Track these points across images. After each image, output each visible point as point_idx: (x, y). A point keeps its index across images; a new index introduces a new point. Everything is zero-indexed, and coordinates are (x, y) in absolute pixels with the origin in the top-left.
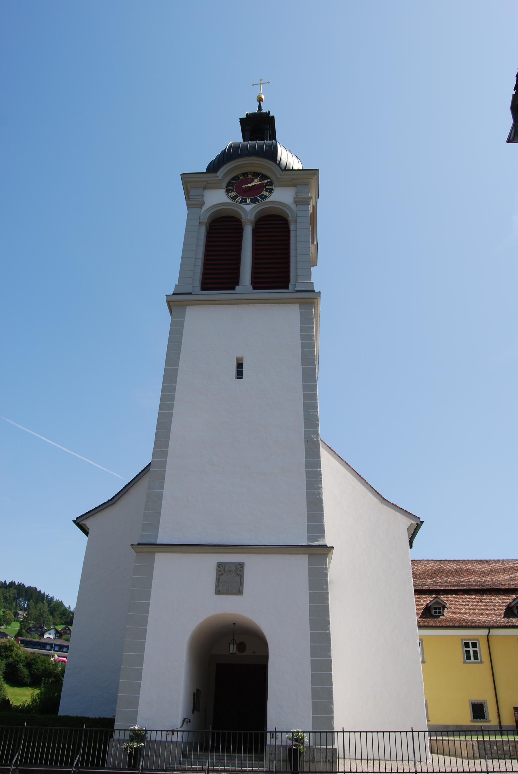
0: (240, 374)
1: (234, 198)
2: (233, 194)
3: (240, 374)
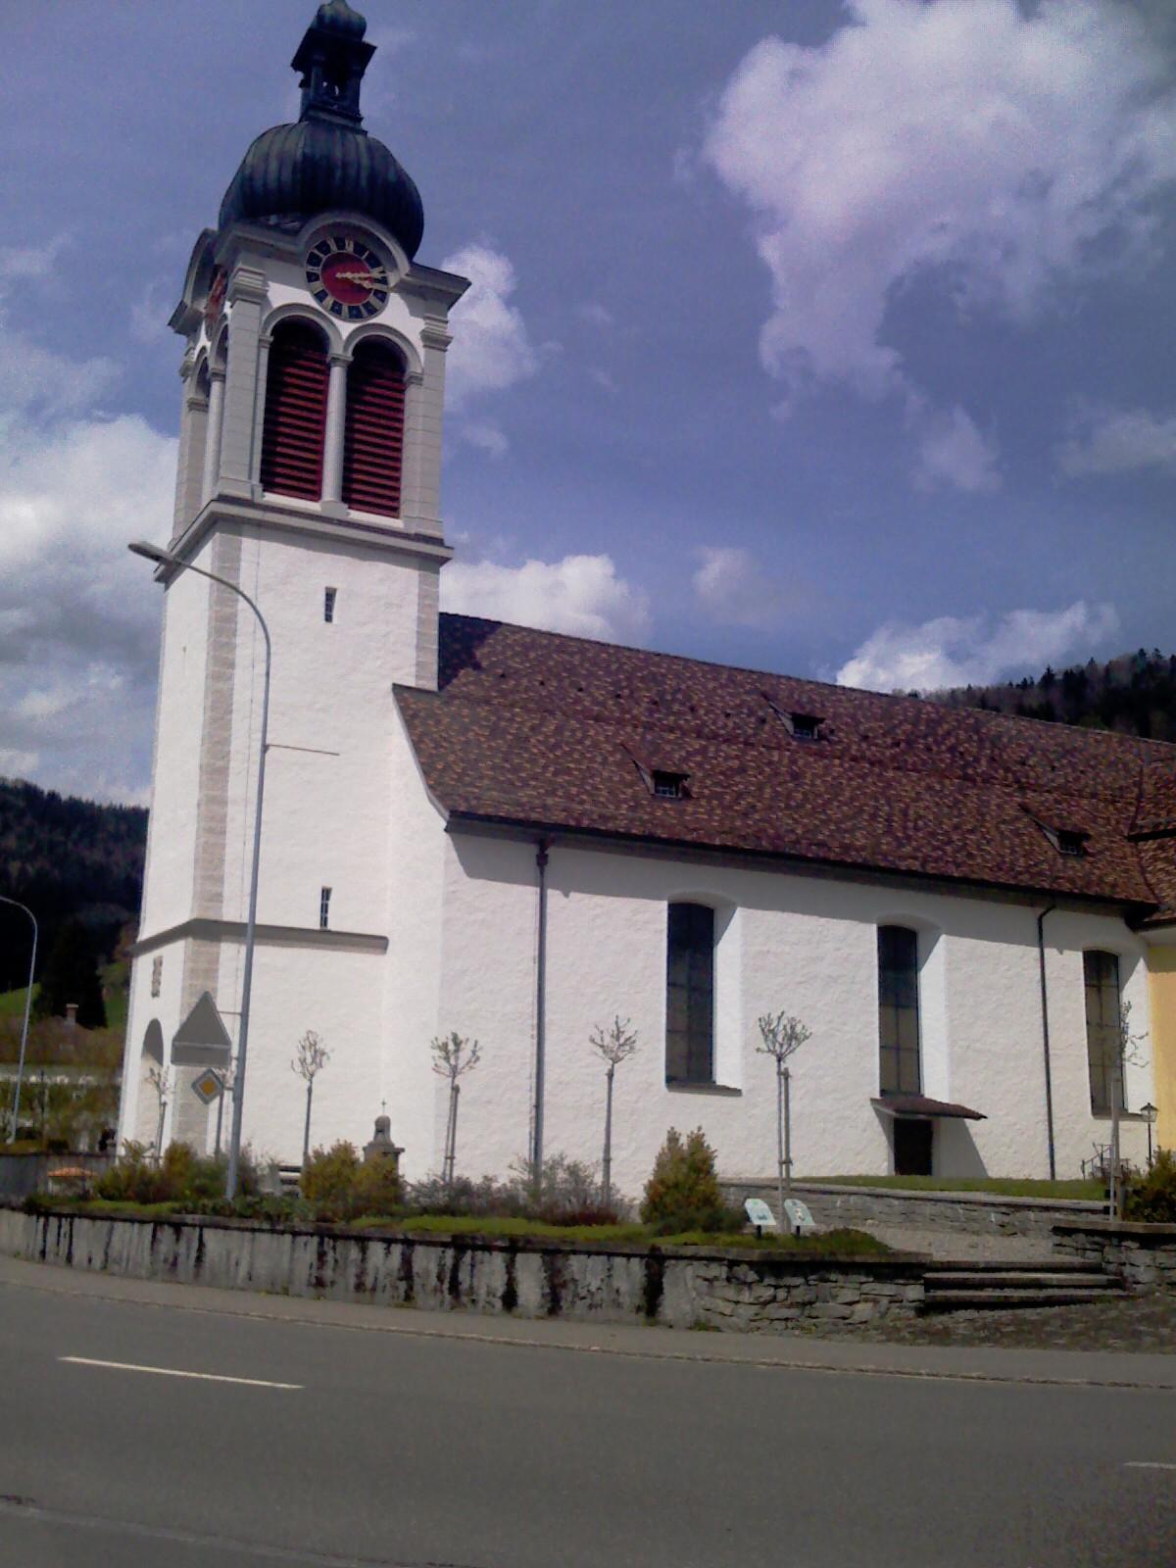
0: (330, 596)
1: (320, 297)
2: (319, 285)
3: (330, 596)
